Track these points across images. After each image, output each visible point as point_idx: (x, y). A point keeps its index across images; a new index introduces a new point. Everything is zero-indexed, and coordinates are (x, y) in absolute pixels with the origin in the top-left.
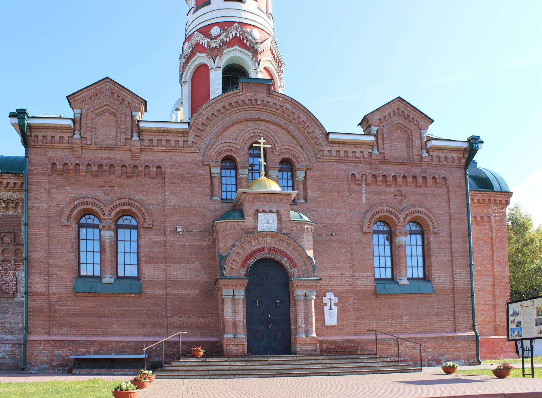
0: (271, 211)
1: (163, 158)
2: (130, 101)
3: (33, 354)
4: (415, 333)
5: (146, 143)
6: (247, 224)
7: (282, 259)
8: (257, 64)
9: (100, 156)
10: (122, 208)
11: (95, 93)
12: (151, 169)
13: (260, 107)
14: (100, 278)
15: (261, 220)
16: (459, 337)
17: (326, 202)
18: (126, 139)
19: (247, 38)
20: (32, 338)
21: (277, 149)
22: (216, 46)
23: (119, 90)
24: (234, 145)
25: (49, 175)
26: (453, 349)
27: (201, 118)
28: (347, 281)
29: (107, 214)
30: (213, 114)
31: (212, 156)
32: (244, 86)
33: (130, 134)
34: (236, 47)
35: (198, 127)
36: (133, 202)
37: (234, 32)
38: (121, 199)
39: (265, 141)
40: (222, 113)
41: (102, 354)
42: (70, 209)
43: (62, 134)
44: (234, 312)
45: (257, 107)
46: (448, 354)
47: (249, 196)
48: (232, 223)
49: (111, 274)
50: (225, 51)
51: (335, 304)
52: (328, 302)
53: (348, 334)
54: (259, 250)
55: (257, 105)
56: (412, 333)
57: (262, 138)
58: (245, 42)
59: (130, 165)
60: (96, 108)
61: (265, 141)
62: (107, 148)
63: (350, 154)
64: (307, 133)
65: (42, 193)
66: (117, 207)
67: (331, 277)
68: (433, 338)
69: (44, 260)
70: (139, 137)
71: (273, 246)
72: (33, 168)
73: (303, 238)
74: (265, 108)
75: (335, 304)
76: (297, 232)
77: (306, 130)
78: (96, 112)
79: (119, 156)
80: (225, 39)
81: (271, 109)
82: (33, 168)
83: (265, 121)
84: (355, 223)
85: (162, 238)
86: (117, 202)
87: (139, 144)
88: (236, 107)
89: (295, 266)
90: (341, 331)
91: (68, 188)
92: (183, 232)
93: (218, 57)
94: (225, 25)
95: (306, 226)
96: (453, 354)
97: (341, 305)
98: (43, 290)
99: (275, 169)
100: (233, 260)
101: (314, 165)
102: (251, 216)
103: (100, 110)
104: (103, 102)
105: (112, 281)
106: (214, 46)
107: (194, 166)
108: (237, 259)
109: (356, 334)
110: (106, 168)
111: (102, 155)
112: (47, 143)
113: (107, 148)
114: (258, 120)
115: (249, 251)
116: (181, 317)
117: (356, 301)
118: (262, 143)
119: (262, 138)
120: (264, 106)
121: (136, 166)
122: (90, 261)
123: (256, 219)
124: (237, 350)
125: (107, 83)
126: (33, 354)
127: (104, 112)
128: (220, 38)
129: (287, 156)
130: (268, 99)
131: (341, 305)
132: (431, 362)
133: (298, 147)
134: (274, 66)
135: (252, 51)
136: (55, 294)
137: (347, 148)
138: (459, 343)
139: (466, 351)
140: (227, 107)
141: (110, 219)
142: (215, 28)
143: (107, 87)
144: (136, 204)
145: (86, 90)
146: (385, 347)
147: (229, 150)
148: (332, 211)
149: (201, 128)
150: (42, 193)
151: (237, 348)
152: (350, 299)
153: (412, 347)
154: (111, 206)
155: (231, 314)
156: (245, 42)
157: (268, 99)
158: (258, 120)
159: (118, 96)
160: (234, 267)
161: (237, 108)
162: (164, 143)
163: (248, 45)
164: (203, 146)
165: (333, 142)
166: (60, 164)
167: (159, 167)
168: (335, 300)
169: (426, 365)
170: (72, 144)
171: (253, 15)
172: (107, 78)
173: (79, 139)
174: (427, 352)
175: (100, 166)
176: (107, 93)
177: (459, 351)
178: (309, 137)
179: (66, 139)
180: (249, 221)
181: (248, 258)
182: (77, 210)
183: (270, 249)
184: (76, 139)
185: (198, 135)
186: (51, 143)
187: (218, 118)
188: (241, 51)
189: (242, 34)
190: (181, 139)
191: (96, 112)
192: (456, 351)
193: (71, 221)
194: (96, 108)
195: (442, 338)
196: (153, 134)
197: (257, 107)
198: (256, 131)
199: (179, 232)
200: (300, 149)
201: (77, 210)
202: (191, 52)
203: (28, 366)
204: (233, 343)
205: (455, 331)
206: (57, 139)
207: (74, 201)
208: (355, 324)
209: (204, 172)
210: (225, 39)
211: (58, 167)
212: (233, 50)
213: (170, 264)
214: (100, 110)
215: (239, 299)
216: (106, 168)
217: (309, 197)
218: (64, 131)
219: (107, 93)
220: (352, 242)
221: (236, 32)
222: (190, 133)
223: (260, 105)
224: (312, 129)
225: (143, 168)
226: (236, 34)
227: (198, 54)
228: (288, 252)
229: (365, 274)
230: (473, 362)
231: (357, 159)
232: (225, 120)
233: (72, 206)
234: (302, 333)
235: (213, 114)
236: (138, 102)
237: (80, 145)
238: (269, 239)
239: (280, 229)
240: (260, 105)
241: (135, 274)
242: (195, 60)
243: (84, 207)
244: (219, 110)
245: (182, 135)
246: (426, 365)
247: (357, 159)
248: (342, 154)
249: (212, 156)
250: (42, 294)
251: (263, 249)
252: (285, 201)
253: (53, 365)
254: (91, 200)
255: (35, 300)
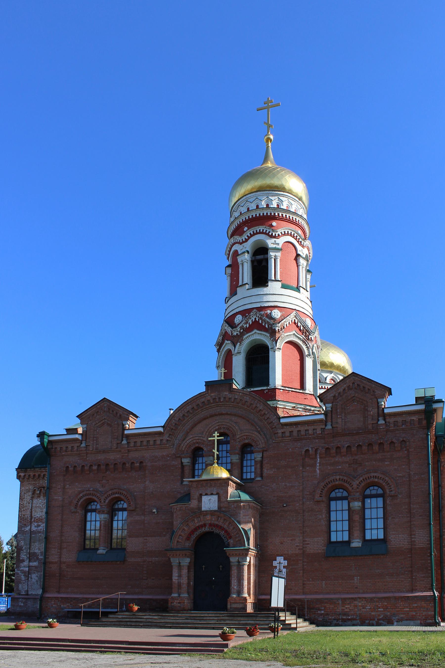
0: (212, 494)
1: (145, 455)
2: (121, 413)
3: (47, 607)
4: (367, 593)
5: (132, 444)
6: (192, 506)
7: (220, 533)
8: (274, 343)
9: (99, 458)
10: (114, 496)
11: (97, 411)
12: (136, 465)
13: (223, 403)
14: (348, 543)
15: (204, 502)
16: (416, 596)
17: (280, 478)
18: (118, 443)
19: (265, 321)
20: (47, 595)
21: (238, 437)
22: (237, 334)
23: (113, 406)
24: (201, 438)
25: (64, 476)
26: (408, 609)
27: (174, 420)
28: (297, 546)
29: (102, 502)
30: (184, 415)
31: (183, 449)
32: (209, 388)
33: (121, 439)
34: (255, 331)
35: (172, 427)
36: (122, 492)
37: (253, 317)
38: (113, 489)
39: (218, 434)
40: (191, 413)
41: (94, 608)
42: (77, 500)
43: (73, 445)
44: (180, 576)
45: (221, 403)
46: (402, 614)
47: (194, 483)
48: (181, 506)
49: (105, 547)
50: (245, 337)
51: (284, 567)
52: (277, 565)
53: (296, 594)
54: (201, 526)
55: (221, 402)
56: (364, 593)
57: (216, 432)
58: (264, 324)
59: (120, 463)
60: (97, 422)
61: (218, 434)
62: (104, 452)
63: (303, 433)
64: (264, 419)
65: (59, 489)
66: (110, 496)
67: (282, 543)
68: (385, 598)
69: (58, 538)
70: (127, 441)
71: (213, 522)
72: (54, 471)
73: (240, 514)
74: (228, 403)
75: (284, 567)
76: (235, 509)
77: (263, 417)
78: (97, 425)
79: (113, 457)
80: (245, 326)
81: (232, 404)
82: (54, 471)
83: (227, 414)
84: (308, 493)
85: (143, 517)
86: (110, 492)
87: (126, 446)
88: (203, 407)
89: (230, 537)
90: (289, 591)
91: (77, 484)
92: (157, 512)
93: (239, 343)
94: (245, 313)
95: (242, 504)
96: (408, 613)
97: (291, 567)
98: (56, 560)
99: (235, 454)
100: (180, 535)
101: (271, 446)
102: (195, 499)
103: (100, 423)
104: (102, 417)
105: (360, 545)
106: (235, 334)
107: (169, 459)
108: (182, 534)
109: (304, 593)
110: (103, 467)
111: (101, 457)
112: (63, 452)
113: (104, 452)
114: (222, 414)
115: (193, 527)
116: (153, 579)
117: (305, 564)
118: (216, 437)
119: (216, 432)
120: (227, 402)
121: (124, 464)
122: (340, 518)
123: (200, 500)
124: (179, 606)
125: (105, 402)
126: (47, 607)
127: (103, 424)
128: (240, 326)
129: (247, 441)
130: (230, 396)
131: (291, 567)
132: (380, 622)
133: (256, 433)
134: (299, 338)
135: (270, 331)
136: (64, 563)
137: (300, 428)
138: (415, 604)
139: (424, 611)
140: (195, 408)
141: (105, 505)
142: (237, 316)
143: (105, 405)
144: (124, 492)
145: (90, 410)
146: (332, 606)
147: (197, 443)
148: (285, 485)
149: (174, 428)
150: (59, 489)
151: (179, 605)
152: (300, 562)
153: (361, 606)
154: (106, 495)
155: (177, 578)
156: (264, 324)
157: (230, 396)
158: (222, 414)
159: (113, 411)
160: (180, 540)
161: (204, 407)
162: (145, 443)
163: (267, 326)
164: (176, 442)
165: (286, 424)
166: (71, 467)
167: (141, 463)
168: (285, 563)
169: (375, 624)
170: (80, 451)
171: (274, 296)
172: (105, 398)
173: (84, 447)
174: (378, 611)
175: (99, 465)
176: (105, 409)
177: (415, 611)
178: (266, 423)
179: (76, 448)
180: (194, 503)
181: (192, 532)
182: (82, 500)
183: (210, 525)
184: (82, 447)
185: (171, 433)
186: (66, 452)
187: (188, 418)
188: (260, 334)
189: (260, 318)
190: (158, 439)
191: (97, 425)
192: (412, 611)
193: (78, 508)
194: (97, 422)
195: (396, 598)
196: (136, 437)
197: (221, 403)
198: (220, 423)
199: (154, 512)
200: (257, 434)
201: (82, 500)
202: (222, 339)
203: (43, 616)
204: (176, 601)
205: (412, 591)
206: (70, 448)
207: (80, 494)
208: (304, 584)
209: (176, 463)
210: (245, 326)
211: (70, 469)
212: (253, 334)
213: (147, 538)
214: (100, 423)
215: (183, 566)
216: (103, 467)
217: (264, 475)
218: (74, 442)
219: (105, 409)
220: (304, 511)
221: (255, 317)
222: (165, 433)
223: (222, 402)
224: (268, 416)
225: (130, 464)
226: (255, 319)
227: (226, 342)
228: (225, 527)
229: (316, 539)
230: (430, 623)
231: (310, 436)
232: (194, 418)
233: (79, 497)
234: (234, 593)
235: (184, 415)
236: (127, 413)
237: (85, 452)
238: (208, 517)
239: (219, 507)
240: (222, 402)
241: (381, 536)
242: (225, 347)
243: (87, 497)
244: (189, 411)
245: (159, 435)
246: (375, 624)
247: (310, 436)
248: (295, 434)
249: (183, 449)
250: (56, 563)
251: (205, 525)
252: (223, 485)
253: (59, 615)
254: (92, 492)
255: (51, 568)
